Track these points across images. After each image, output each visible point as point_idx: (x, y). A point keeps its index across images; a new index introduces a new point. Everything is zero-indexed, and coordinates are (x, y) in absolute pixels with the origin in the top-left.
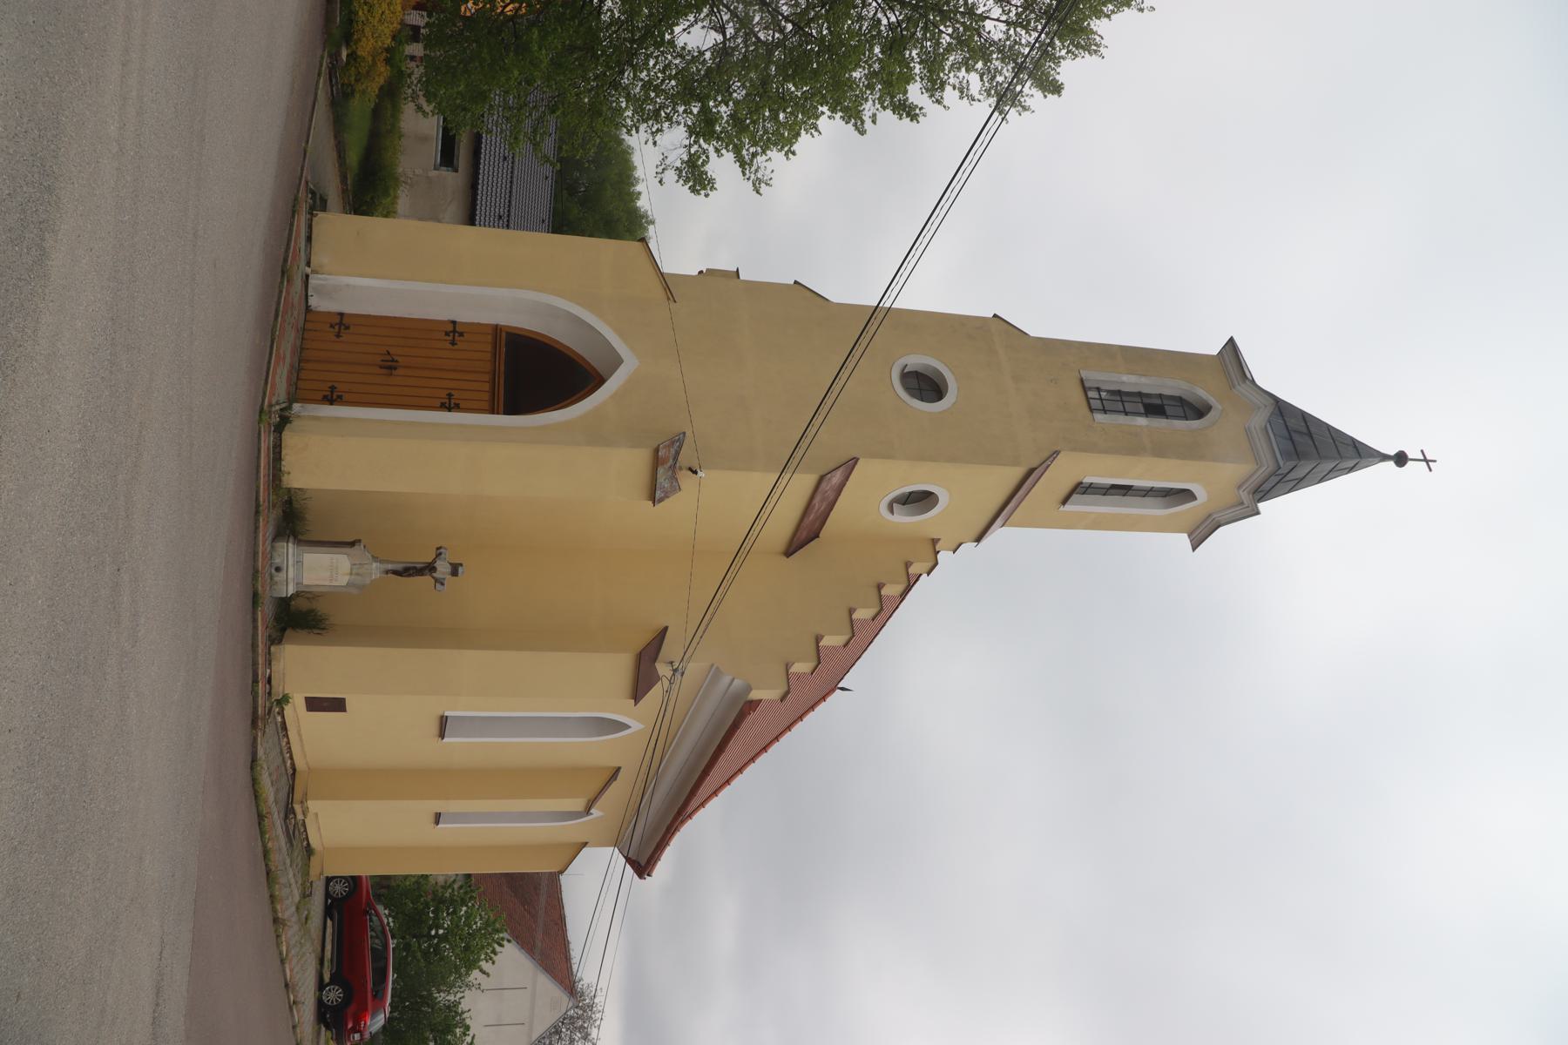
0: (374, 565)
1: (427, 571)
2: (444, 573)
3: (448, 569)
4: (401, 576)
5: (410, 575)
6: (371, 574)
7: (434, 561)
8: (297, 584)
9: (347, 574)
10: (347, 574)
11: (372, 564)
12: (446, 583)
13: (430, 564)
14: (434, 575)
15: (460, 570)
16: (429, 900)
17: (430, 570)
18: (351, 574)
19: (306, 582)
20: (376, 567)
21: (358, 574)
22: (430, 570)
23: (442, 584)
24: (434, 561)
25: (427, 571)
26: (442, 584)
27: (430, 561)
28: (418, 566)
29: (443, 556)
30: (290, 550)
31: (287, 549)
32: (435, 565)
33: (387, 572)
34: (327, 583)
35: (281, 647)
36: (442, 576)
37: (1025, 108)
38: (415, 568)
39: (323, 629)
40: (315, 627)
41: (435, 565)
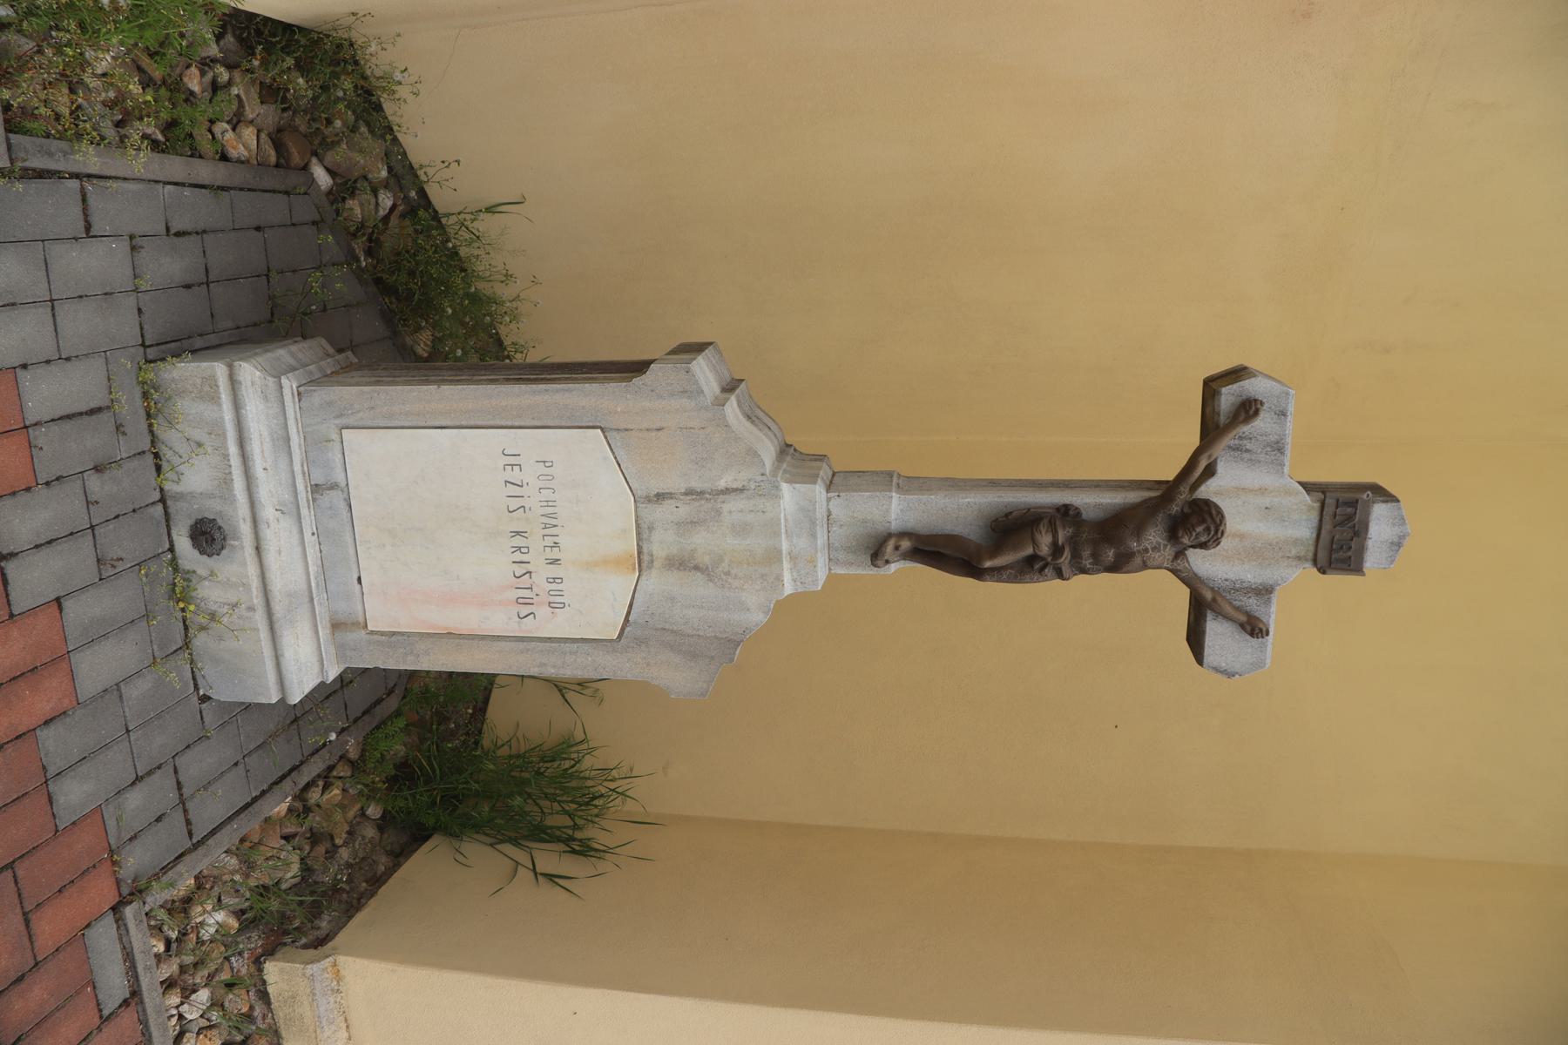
0: (790, 496)
1: (1154, 536)
2: (1260, 552)
3: (1299, 523)
4: (974, 571)
5: (1032, 567)
6: (773, 557)
7: (1198, 468)
8: (336, 626)
9: (616, 563)
10: (616, 563)
11: (775, 493)
12: (1273, 616)
13: (1169, 489)
14: (1202, 562)
15: (1380, 524)
16: (1086, 534)
17: (1175, 529)
18: (642, 562)
19: (381, 615)
20: (807, 512)
21: (681, 563)
22: (1175, 529)
23: (1254, 628)
24: (1198, 468)
25: (1154, 536)
26: (1254, 628)
27: (1170, 474)
28: (1089, 503)
29: (1262, 424)
30: (256, 412)
31: (237, 406)
32: (1207, 491)
33: (876, 549)
34: (501, 621)
35: (320, 969)
36: (1250, 574)
37: (607, 851)
38: (1066, 513)
39: (585, 850)
40: (541, 834)
41: (1207, 491)
